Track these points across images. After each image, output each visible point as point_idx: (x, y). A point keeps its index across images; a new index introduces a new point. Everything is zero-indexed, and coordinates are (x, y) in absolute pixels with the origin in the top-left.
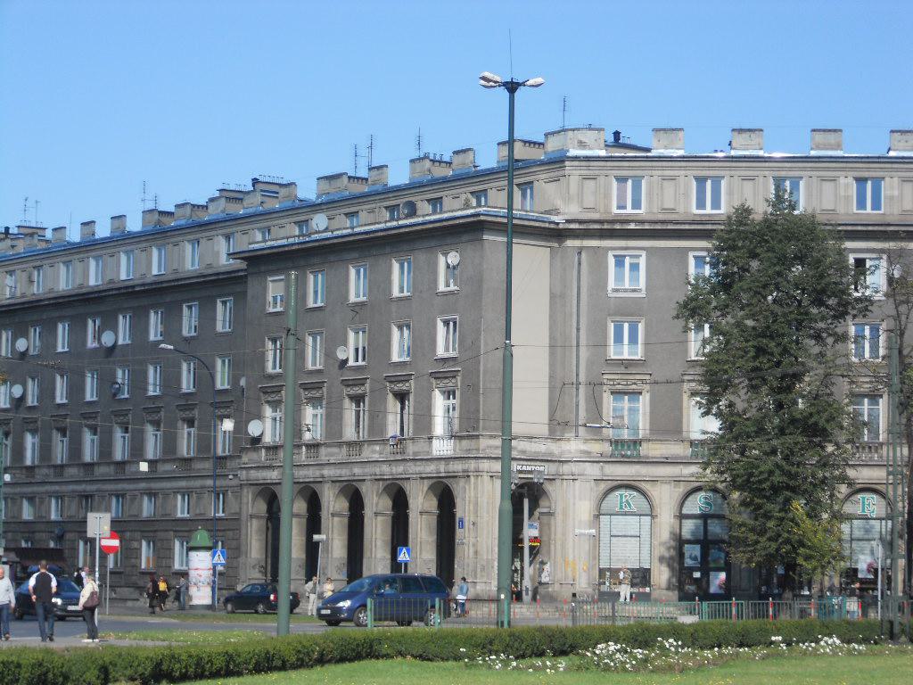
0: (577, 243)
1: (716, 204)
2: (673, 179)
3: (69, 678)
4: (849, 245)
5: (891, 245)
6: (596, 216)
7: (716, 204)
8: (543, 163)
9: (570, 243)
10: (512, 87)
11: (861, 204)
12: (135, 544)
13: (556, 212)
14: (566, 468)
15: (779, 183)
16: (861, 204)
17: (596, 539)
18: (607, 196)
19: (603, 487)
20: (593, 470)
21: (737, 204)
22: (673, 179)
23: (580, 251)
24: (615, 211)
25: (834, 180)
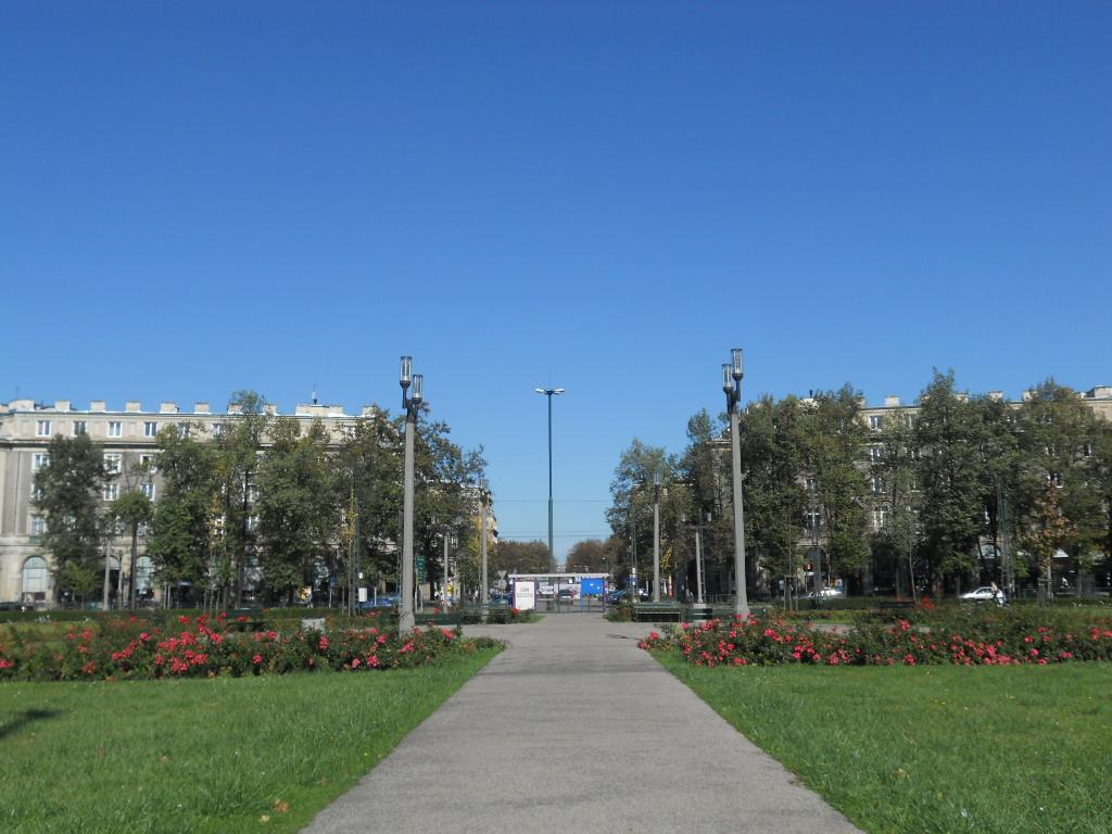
0: (18, 449)
1: (47, 433)
2: (63, 422)
3: (802, 662)
4: (105, 450)
5: (122, 450)
6: (28, 438)
7: (47, 433)
8: (6, 414)
9: (14, 449)
10: (550, 393)
11: (147, 433)
12: (968, 610)
13: (10, 436)
14: (8, 549)
15: (77, 423)
16: (147, 433)
17: (21, 580)
18: (33, 429)
19: (25, 557)
20: (20, 549)
21: (55, 433)
22: (63, 422)
23: (19, 453)
24: (37, 436)
25: (135, 423)
